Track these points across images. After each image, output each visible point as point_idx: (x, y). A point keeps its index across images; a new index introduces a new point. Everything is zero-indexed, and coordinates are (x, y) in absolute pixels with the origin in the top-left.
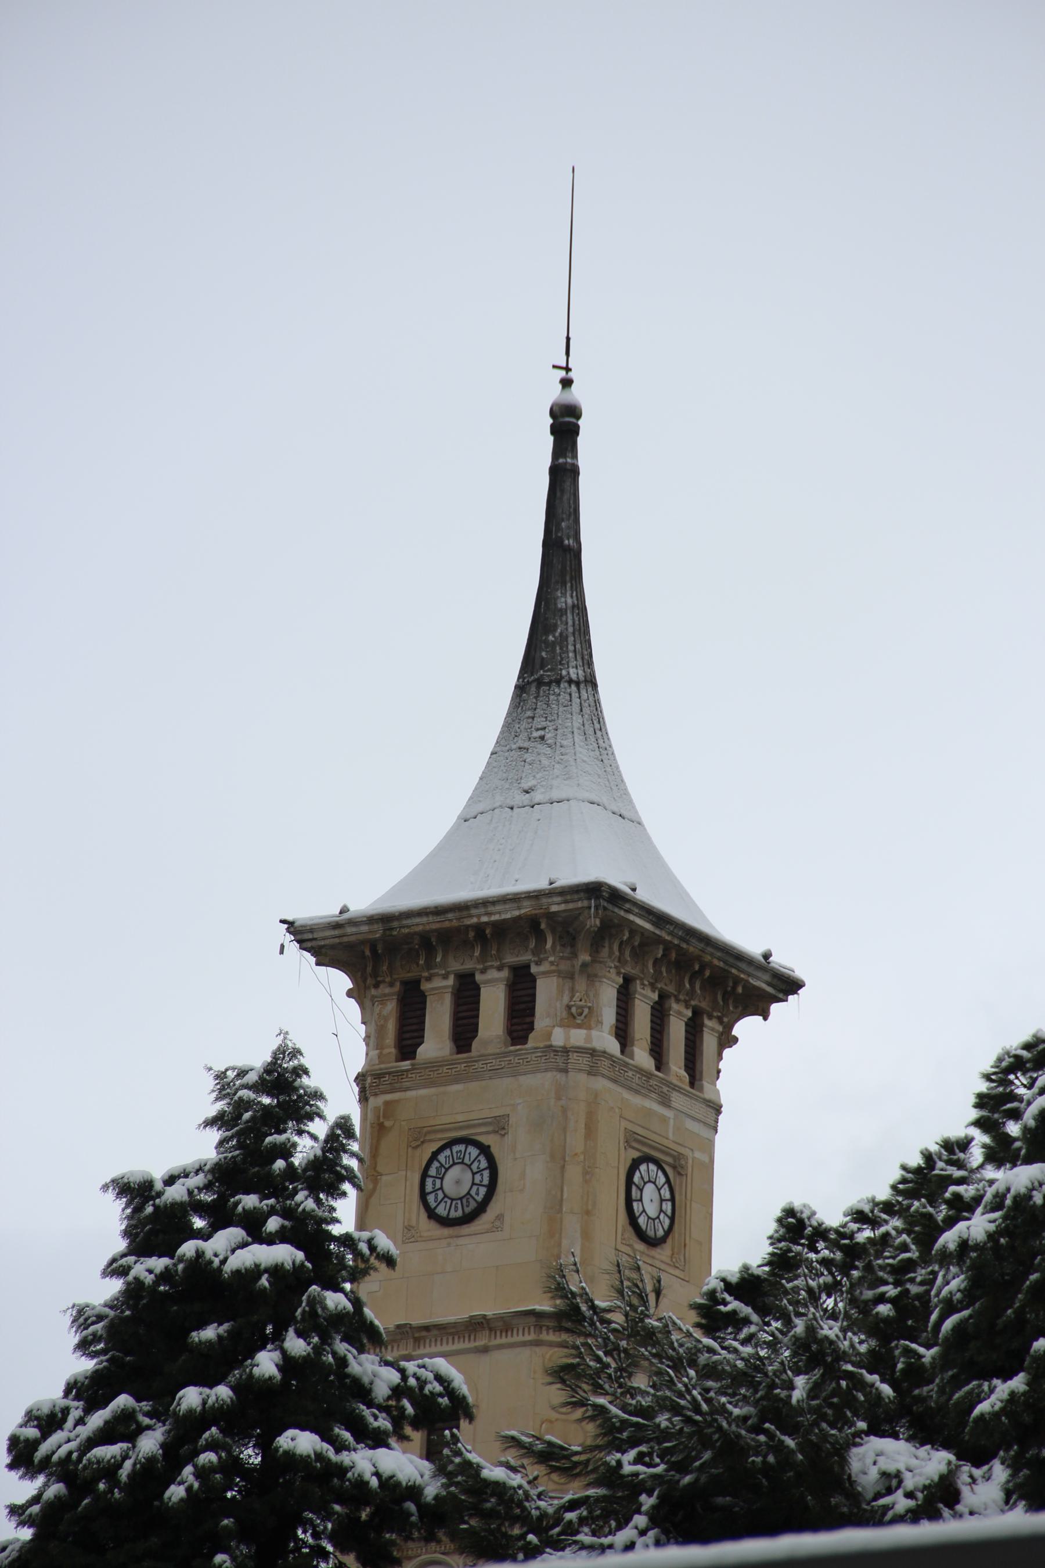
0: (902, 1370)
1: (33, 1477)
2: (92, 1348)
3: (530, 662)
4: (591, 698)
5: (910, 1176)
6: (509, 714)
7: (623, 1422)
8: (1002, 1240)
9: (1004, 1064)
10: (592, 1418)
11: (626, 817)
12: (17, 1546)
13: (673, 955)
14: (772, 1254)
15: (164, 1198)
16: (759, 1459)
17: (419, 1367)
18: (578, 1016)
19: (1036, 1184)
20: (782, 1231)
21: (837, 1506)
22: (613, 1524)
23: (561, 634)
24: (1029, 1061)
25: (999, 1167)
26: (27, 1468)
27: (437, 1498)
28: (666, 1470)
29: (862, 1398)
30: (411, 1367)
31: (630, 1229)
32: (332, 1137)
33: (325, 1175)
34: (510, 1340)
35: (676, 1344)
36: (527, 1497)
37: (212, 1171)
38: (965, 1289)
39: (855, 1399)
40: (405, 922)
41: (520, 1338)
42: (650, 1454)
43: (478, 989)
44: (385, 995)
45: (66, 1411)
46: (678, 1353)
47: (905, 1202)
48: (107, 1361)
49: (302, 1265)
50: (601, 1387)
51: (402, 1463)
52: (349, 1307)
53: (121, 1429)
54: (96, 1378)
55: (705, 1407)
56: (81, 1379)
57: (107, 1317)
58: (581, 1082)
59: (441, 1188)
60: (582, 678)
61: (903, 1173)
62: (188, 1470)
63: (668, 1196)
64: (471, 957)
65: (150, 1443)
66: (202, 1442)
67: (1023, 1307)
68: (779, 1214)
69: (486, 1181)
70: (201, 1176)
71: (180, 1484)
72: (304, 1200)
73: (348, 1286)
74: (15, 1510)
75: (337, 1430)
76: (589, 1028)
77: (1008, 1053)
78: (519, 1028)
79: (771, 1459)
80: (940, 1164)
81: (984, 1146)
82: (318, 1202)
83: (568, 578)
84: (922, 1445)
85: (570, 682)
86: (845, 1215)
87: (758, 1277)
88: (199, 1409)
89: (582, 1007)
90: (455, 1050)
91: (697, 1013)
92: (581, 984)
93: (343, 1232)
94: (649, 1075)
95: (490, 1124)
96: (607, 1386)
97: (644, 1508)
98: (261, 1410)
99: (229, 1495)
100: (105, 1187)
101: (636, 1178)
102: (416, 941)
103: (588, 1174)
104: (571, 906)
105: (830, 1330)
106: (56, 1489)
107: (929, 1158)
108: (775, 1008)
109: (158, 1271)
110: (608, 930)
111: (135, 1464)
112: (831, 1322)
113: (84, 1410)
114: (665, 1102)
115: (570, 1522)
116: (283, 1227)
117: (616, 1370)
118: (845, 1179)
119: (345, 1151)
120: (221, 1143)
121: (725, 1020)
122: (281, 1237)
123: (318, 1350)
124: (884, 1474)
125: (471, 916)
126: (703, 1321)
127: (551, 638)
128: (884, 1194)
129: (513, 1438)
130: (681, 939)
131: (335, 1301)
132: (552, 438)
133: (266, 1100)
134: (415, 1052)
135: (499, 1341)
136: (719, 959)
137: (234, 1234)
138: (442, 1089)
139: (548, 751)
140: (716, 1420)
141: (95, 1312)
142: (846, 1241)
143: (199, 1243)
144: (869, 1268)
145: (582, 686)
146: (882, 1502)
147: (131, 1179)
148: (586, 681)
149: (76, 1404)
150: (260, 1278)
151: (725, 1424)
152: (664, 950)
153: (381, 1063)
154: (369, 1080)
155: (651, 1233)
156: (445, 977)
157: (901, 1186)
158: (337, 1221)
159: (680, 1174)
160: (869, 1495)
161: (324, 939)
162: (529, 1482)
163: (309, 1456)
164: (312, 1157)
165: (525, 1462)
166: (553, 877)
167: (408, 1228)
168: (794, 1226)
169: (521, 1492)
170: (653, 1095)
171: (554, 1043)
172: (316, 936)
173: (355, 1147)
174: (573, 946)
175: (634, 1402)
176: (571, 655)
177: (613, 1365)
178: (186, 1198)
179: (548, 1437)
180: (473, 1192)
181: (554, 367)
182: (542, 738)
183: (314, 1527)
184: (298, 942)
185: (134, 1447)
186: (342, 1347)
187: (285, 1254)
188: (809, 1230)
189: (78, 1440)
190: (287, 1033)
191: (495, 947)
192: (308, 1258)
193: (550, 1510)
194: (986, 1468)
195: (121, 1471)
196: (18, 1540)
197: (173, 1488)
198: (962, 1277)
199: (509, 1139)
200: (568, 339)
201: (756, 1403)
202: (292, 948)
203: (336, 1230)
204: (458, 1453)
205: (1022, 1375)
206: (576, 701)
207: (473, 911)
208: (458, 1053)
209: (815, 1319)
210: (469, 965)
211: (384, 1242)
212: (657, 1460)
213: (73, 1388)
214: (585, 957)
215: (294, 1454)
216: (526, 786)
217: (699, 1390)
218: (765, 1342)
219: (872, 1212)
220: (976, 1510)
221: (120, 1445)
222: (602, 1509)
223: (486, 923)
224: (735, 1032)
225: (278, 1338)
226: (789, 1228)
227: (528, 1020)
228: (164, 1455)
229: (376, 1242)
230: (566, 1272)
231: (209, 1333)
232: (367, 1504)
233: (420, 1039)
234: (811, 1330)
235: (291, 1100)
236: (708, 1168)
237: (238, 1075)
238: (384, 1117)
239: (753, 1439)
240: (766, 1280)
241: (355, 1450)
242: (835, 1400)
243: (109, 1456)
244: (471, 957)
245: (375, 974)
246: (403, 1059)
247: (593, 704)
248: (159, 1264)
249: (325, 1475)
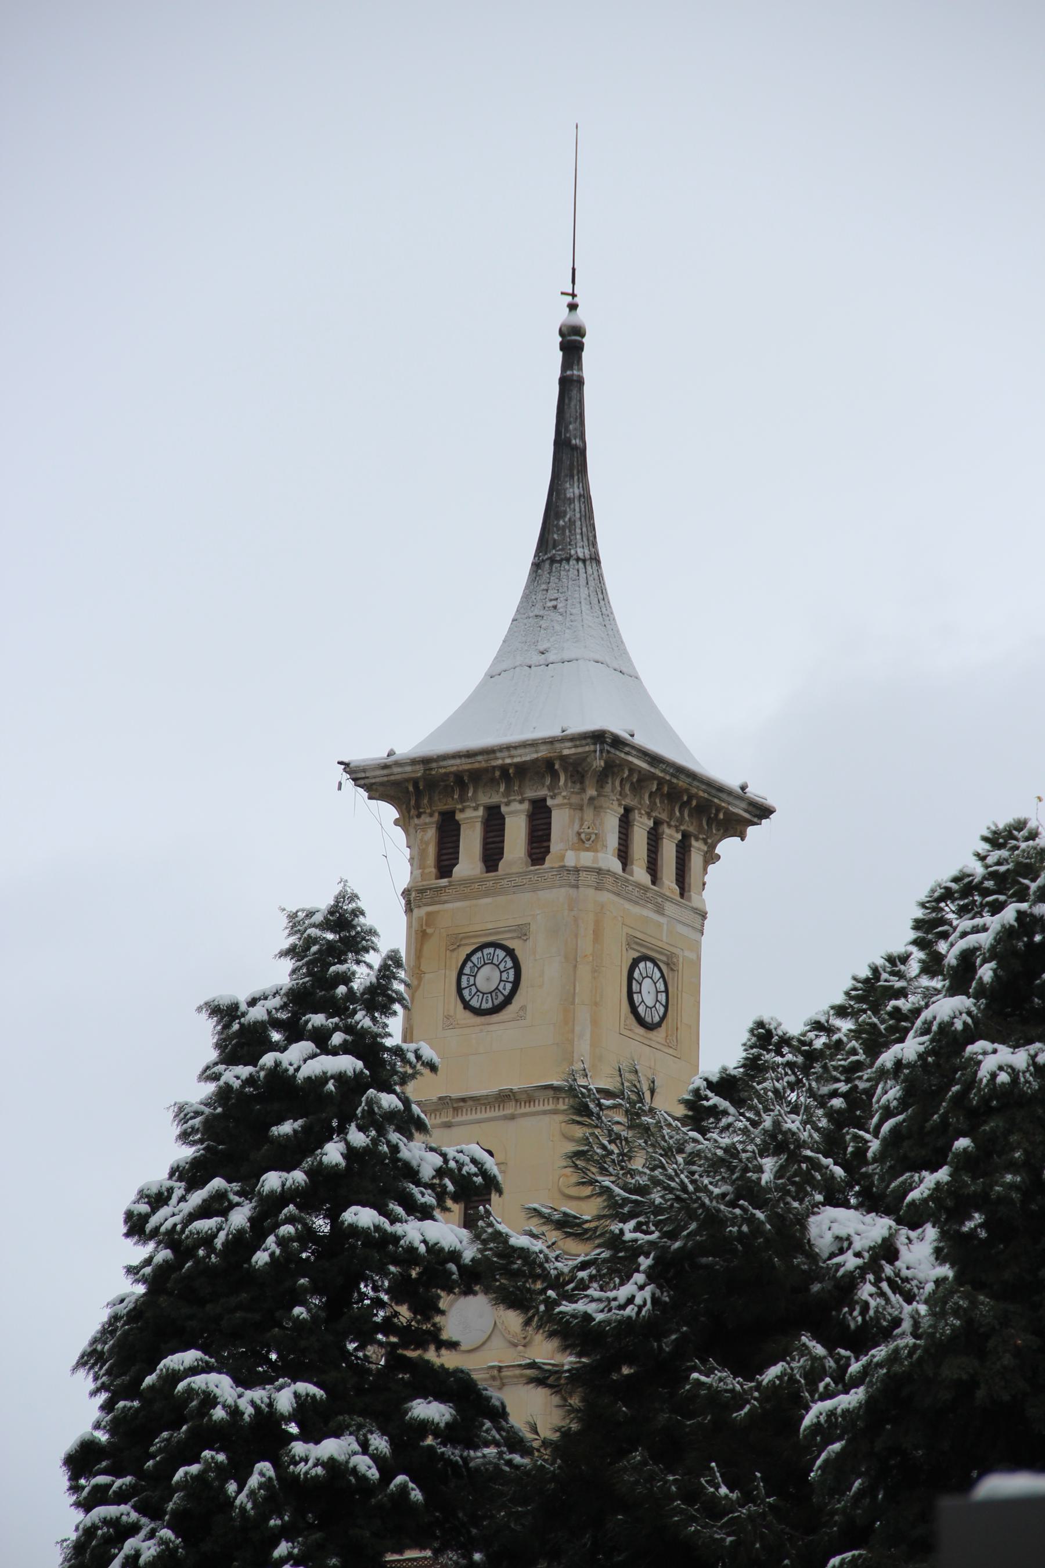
0: (852, 1153)
1: (145, 1243)
2: (191, 1138)
3: (544, 543)
4: (596, 573)
5: (860, 985)
6: (527, 587)
7: (626, 1201)
8: (930, 1059)
9: (936, 894)
10: (600, 1194)
11: (626, 673)
12: (133, 1299)
13: (666, 789)
14: (746, 1059)
15: (248, 1017)
16: (735, 1229)
17: (458, 1152)
18: (585, 841)
19: (957, 1013)
20: (754, 1039)
21: (798, 1265)
22: (617, 1280)
23: (570, 519)
24: (956, 892)
25: (932, 978)
26: (140, 1236)
27: (473, 1260)
28: (659, 1238)
29: (819, 1178)
30: (451, 1152)
31: (631, 1017)
32: (384, 967)
33: (379, 998)
34: (532, 1109)
35: (667, 1137)
36: (547, 1259)
37: (287, 994)
38: (900, 1098)
39: (813, 1177)
40: (442, 763)
41: (541, 1108)
42: (647, 1223)
43: (503, 818)
44: (426, 824)
45: (170, 1191)
46: (669, 1144)
47: (856, 1006)
48: (203, 1149)
49: (361, 1072)
50: (606, 1170)
51: (446, 1231)
52: (400, 1106)
53: (216, 1206)
54: (196, 1163)
55: (691, 1188)
56: (182, 1164)
57: (202, 1113)
58: (589, 895)
59: (474, 984)
60: (588, 556)
61: (854, 982)
62: (271, 1240)
63: (662, 988)
64: (498, 792)
65: (240, 1217)
66: (282, 1216)
67: (946, 1113)
68: (751, 1025)
69: (511, 979)
70: (278, 998)
71: (264, 1250)
72: (362, 1019)
73: (398, 1088)
74: (131, 1270)
75: (391, 1206)
76: (596, 851)
77: (940, 886)
78: (538, 851)
79: (745, 1228)
80: (884, 976)
81: (921, 961)
82: (374, 1020)
83: (575, 472)
84: (868, 1212)
85: (578, 559)
86: (805, 1025)
87: (734, 1076)
88: (279, 1190)
89: (590, 834)
90: (484, 870)
91: (686, 836)
92: (589, 814)
93: (394, 1044)
94: (646, 889)
95: (514, 931)
96: (611, 1169)
97: (642, 1268)
98: (329, 1190)
99: (304, 1255)
100: (199, 1009)
101: (636, 974)
102: (452, 779)
103: (595, 971)
104: (580, 750)
105: (793, 1123)
106: (164, 1254)
107: (875, 971)
108: (751, 830)
109: (244, 1077)
110: (610, 769)
111: (228, 1235)
112: (793, 1116)
113: (185, 1190)
114: (660, 910)
115: (582, 1279)
116: (345, 1041)
117: (619, 1155)
118: (804, 997)
119: (395, 978)
120: (294, 972)
121: (709, 841)
122: (345, 1049)
123: (375, 1142)
124: (838, 1238)
125: (497, 759)
126: (690, 1113)
127: (561, 523)
128: (840, 999)
129: (535, 1209)
130: (672, 775)
131: (388, 1101)
132: (561, 353)
133: (330, 936)
134: (451, 871)
135: (523, 1110)
136: (704, 791)
137: (306, 1046)
138: (474, 902)
139: (560, 618)
140: (699, 1198)
141: (193, 1109)
142: (806, 1048)
143: (277, 1054)
144: (825, 1067)
145: (588, 563)
146: (835, 1260)
147: (221, 1002)
148: (591, 559)
149: (178, 1184)
150: (327, 1083)
151: (707, 1201)
152: (658, 785)
153: (422, 880)
154: (413, 894)
155: (648, 1019)
156: (476, 809)
157: (853, 993)
158: (390, 1035)
159: (672, 970)
160: (825, 1255)
161: (375, 777)
162: (548, 1247)
163: (369, 1228)
164: (368, 984)
165: (544, 1228)
166: (565, 726)
167: (448, 1017)
168: (764, 1036)
169: (541, 1256)
170: (649, 905)
171: (567, 864)
173: (402, 974)
174: (582, 782)
175: (633, 1181)
176: (578, 537)
177: (616, 1151)
178: (266, 1017)
179: (564, 1209)
180: (501, 987)
181: (562, 293)
182: (555, 607)
183: (374, 1282)
184: (353, 780)
185: (227, 1220)
186: (394, 1137)
187: (348, 1064)
188: (775, 1039)
189: (181, 1214)
190: (346, 881)
191: (517, 784)
192: (366, 1066)
193: (566, 1270)
194: (920, 1230)
195: (216, 1240)
196: (134, 1293)
197: (259, 1254)
198: (898, 1087)
199: (530, 943)
200: (574, 270)
201: (733, 1183)
202: (349, 785)
203: (388, 1042)
204: (491, 1225)
205: (946, 1168)
206: (583, 575)
207: (499, 755)
208: (487, 872)
209: (780, 1115)
210: (495, 799)
211: (428, 1053)
212: (653, 1228)
213: (175, 1172)
214: (592, 792)
215: (357, 1227)
216: (542, 649)
217: (686, 1173)
218: (740, 1129)
219: (827, 1022)
220: (911, 1265)
221: (215, 1219)
222: (608, 1268)
223: (510, 764)
224: (717, 851)
225: (342, 1130)
226: (759, 1037)
227: (545, 844)
228: (251, 1227)
229: (421, 1052)
230: (577, 1076)
231: (287, 1128)
232: (417, 1265)
233: (455, 861)
234: (777, 1124)
235: (350, 936)
236: (697, 963)
237: (307, 916)
238: (426, 925)
239: (730, 1212)
240: (740, 1079)
241: (406, 1222)
242: (797, 1179)
243: (206, 1229)
244: (498, 792)
245: (418, 806)
246: (442, 877)
247: (597, 578)
248: (245, 1071)
249: (382, 1245)
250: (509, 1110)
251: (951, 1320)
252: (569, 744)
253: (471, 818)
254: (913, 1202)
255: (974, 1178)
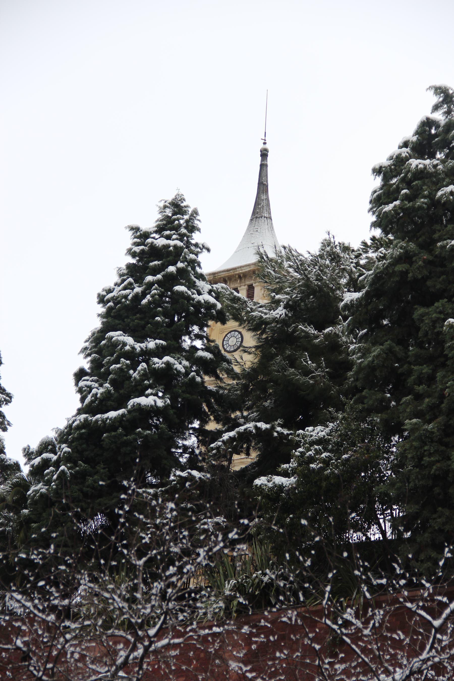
3: (254, 213)
100: (126, 227)
251: (399, 250)
254: (385, 212)
255: (409, 202)
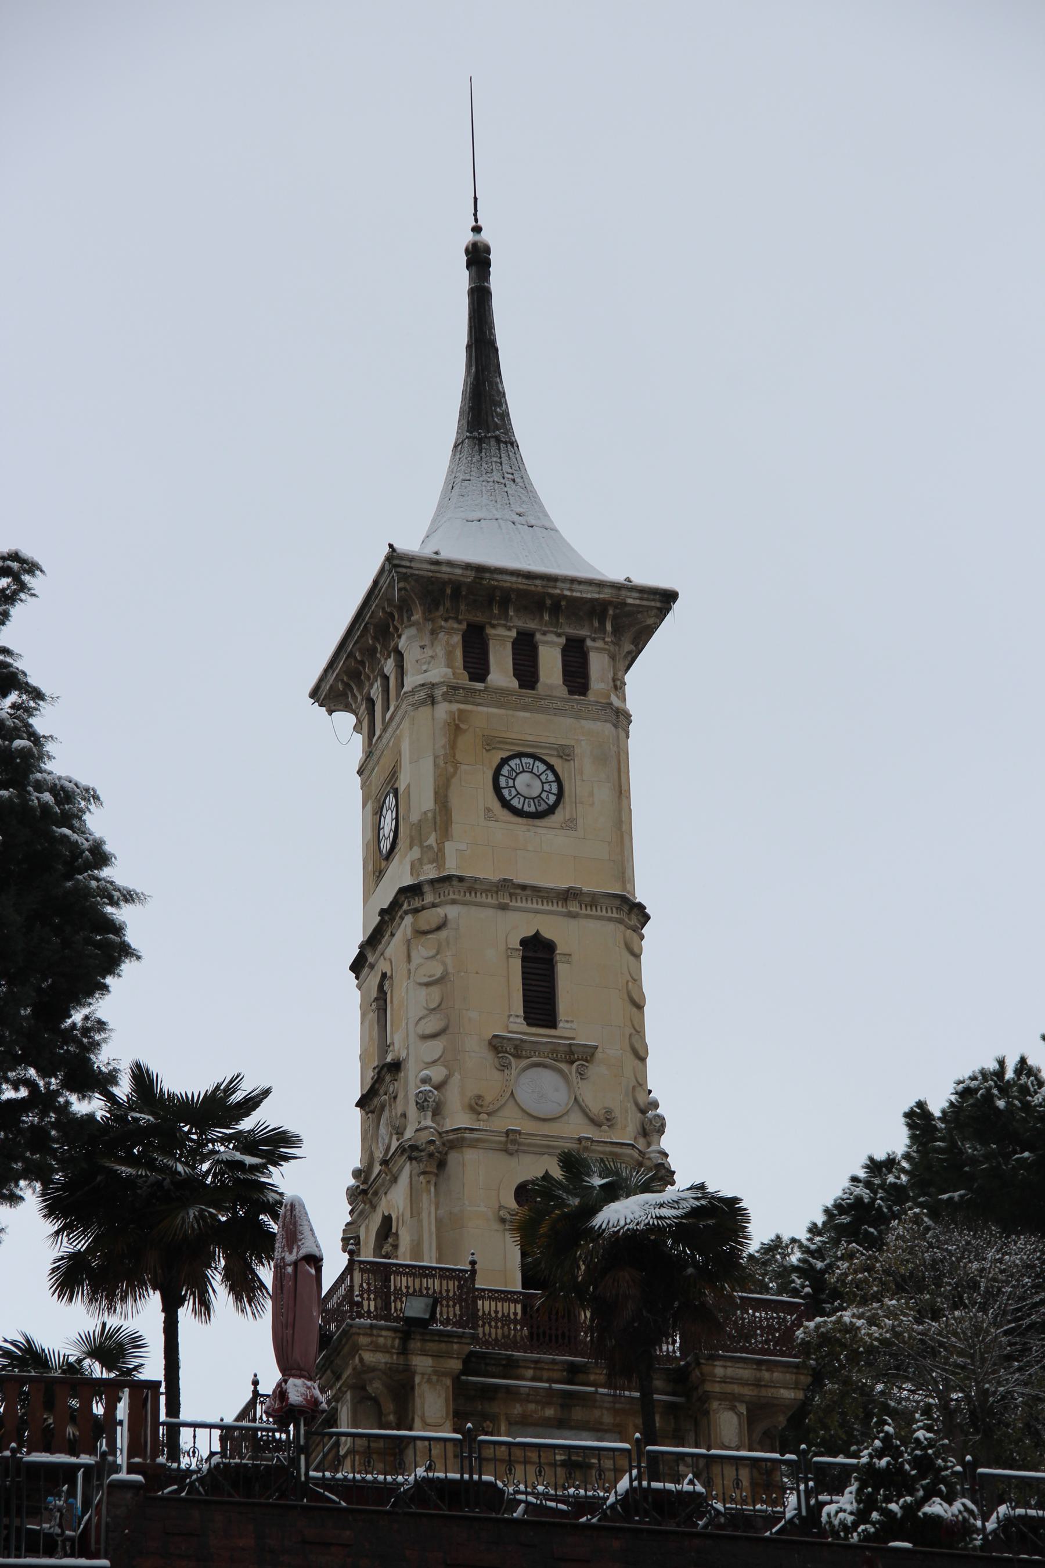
40: (496, 576)
44: (453, 629)
59: (514, 786)
125: (555, 588)
138: (510, 712)
156: (509, 629)
161: (419, 570)
172: (413, 565)
200: (476, 199)
210: (531, 625)
238: (459, 719)
250: (574, 907)
252: (636, 595)
253: (499, 635)
